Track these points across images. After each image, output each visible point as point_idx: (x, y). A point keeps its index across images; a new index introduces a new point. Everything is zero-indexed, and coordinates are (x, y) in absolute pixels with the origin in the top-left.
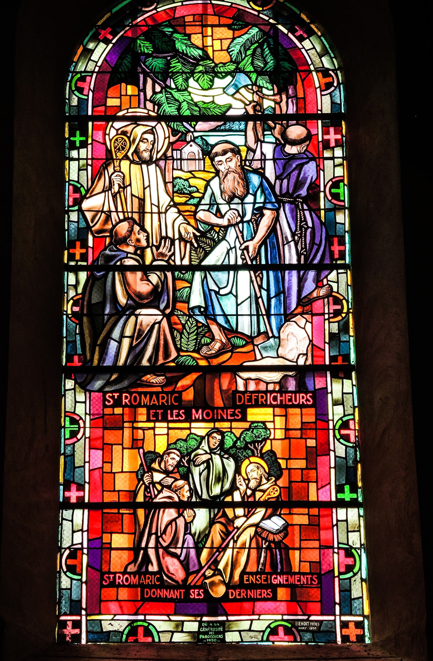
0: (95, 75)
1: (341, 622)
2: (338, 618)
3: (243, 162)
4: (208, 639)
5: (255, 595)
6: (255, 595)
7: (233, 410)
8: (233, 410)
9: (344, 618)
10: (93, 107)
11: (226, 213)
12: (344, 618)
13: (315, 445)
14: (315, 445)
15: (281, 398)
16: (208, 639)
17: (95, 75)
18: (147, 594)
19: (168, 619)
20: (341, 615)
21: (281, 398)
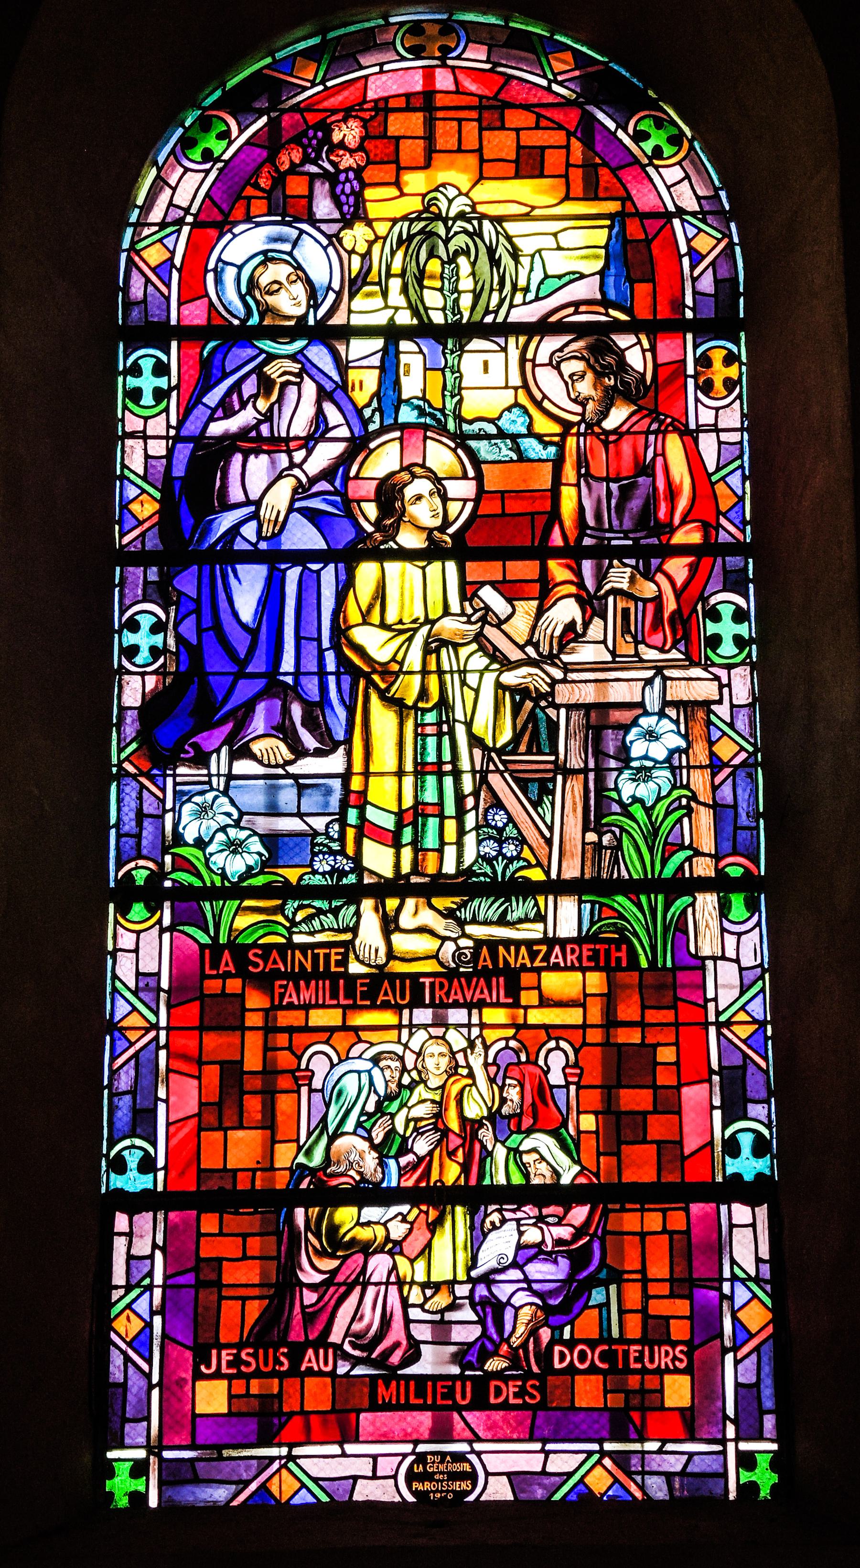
0: (186, 230)
1: (739, 1454)
2: (731, 1447)
3: (444, 719)
4: (434, 1492)
5: (402, 1390)
6: (402, 1390)
7: (235, 1351)
8: (235, 1351)
9: (744, 1446)
10: (180, 304)
11: (620, 180)
12: (744, 1446)
13: (594, 1128)
14: (594, 1128)
15: (618, 954)
16: (434, 1492)
17: (186, 230)
18: (562, 1357)
19: (339, 1452)
20: (737, 1440)
21: (618, 954)
